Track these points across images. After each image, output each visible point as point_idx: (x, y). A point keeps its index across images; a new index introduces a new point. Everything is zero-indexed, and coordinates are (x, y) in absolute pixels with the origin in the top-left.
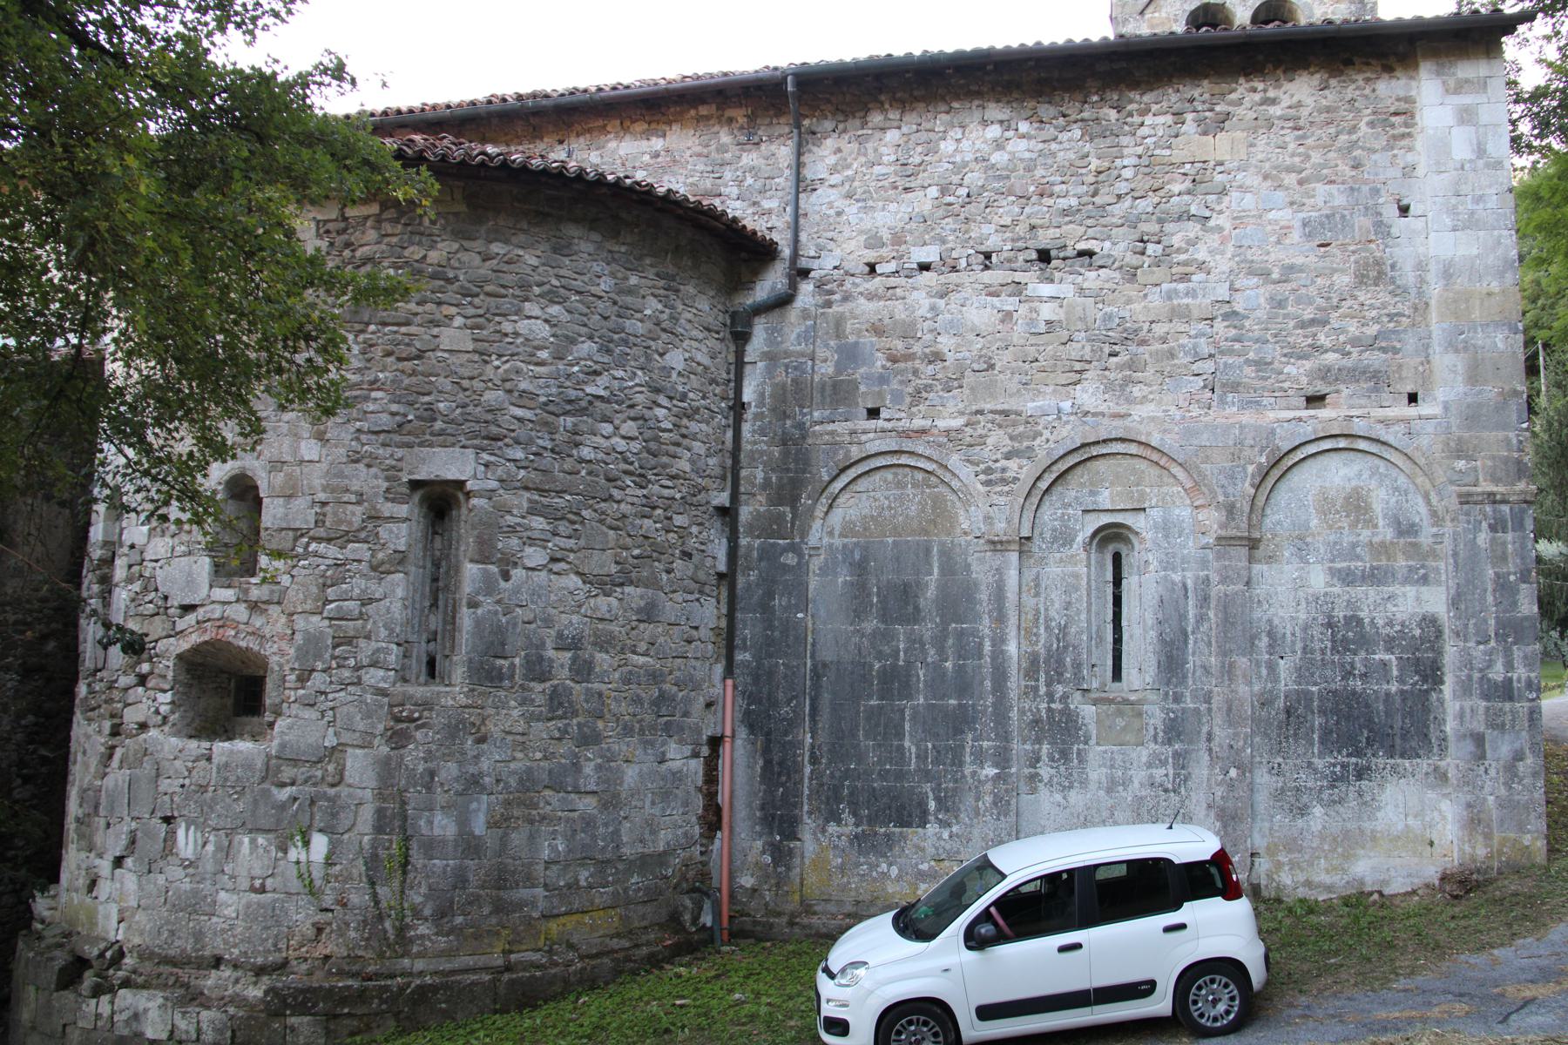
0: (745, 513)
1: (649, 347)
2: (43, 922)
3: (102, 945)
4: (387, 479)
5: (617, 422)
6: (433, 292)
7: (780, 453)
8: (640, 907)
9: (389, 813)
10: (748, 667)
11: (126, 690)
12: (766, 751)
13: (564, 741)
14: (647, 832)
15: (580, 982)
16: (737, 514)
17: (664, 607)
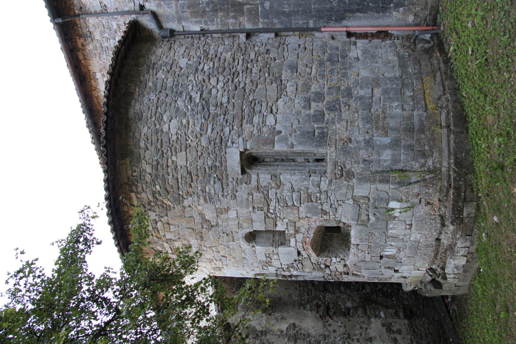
0: (248, 26)
1: (178, 75)
2: (415, 287)
3: (427, 275)
4: (242, 184)
5: (211, 87)
6: (163, 169)
7: (221, 12)
8: (422, 67)
9: (381, 178)
10: (316, 21)
11: (331, 271)
12: (353, 11)
13: (350, 104)
14: (389, 65)
15: (456, 95)
16: (249, 29)
17: (290, 61)
